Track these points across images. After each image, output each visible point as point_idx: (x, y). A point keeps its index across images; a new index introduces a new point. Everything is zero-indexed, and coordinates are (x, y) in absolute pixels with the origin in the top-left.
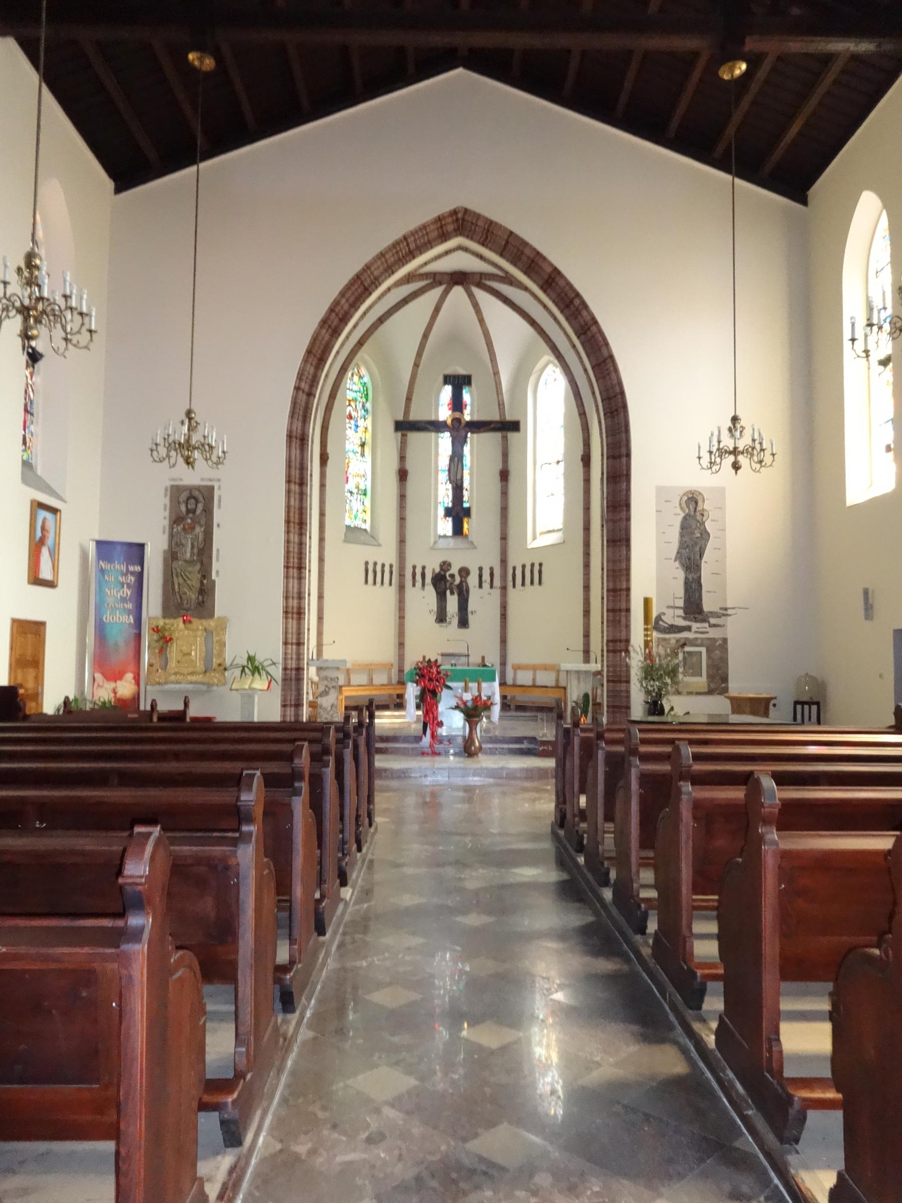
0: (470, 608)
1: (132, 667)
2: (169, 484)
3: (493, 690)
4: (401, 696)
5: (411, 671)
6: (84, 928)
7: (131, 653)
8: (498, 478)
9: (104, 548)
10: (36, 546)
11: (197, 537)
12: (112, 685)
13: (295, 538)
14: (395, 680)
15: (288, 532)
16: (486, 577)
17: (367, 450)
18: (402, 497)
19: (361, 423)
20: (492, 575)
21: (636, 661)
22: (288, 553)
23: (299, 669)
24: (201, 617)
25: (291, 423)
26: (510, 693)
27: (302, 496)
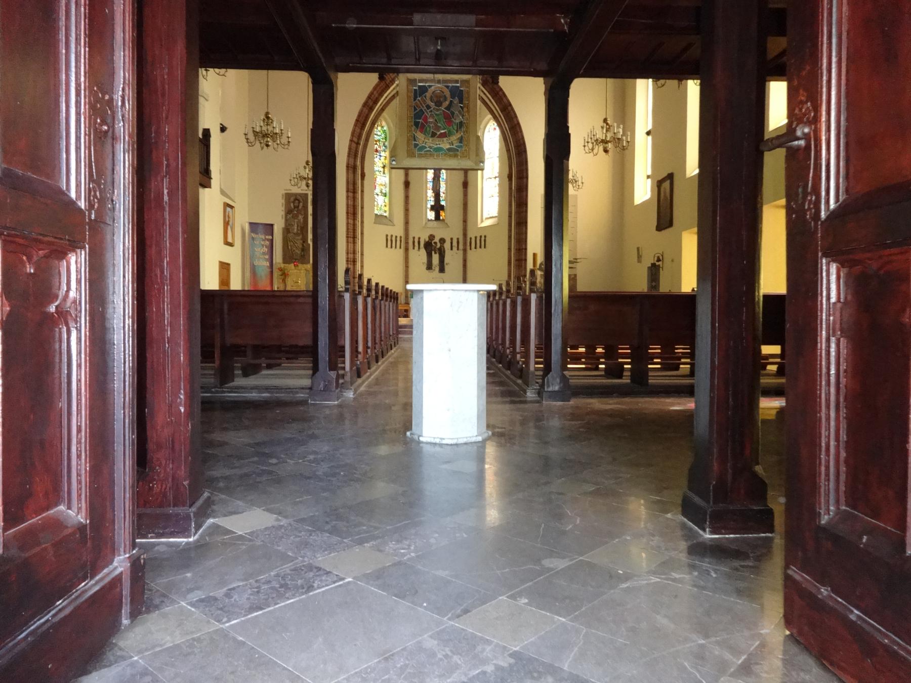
2: (284, 192)
6: (65, 617)
9: (254, 226)
10: (226, 224)
13: (351, 221)
15: (348, 218)
16: (455, 244)
18: (407, 197)
19: (383, 154)
22: (348, 229)
24: (302, 263)
25: (348, 160)
27: (354, 199)
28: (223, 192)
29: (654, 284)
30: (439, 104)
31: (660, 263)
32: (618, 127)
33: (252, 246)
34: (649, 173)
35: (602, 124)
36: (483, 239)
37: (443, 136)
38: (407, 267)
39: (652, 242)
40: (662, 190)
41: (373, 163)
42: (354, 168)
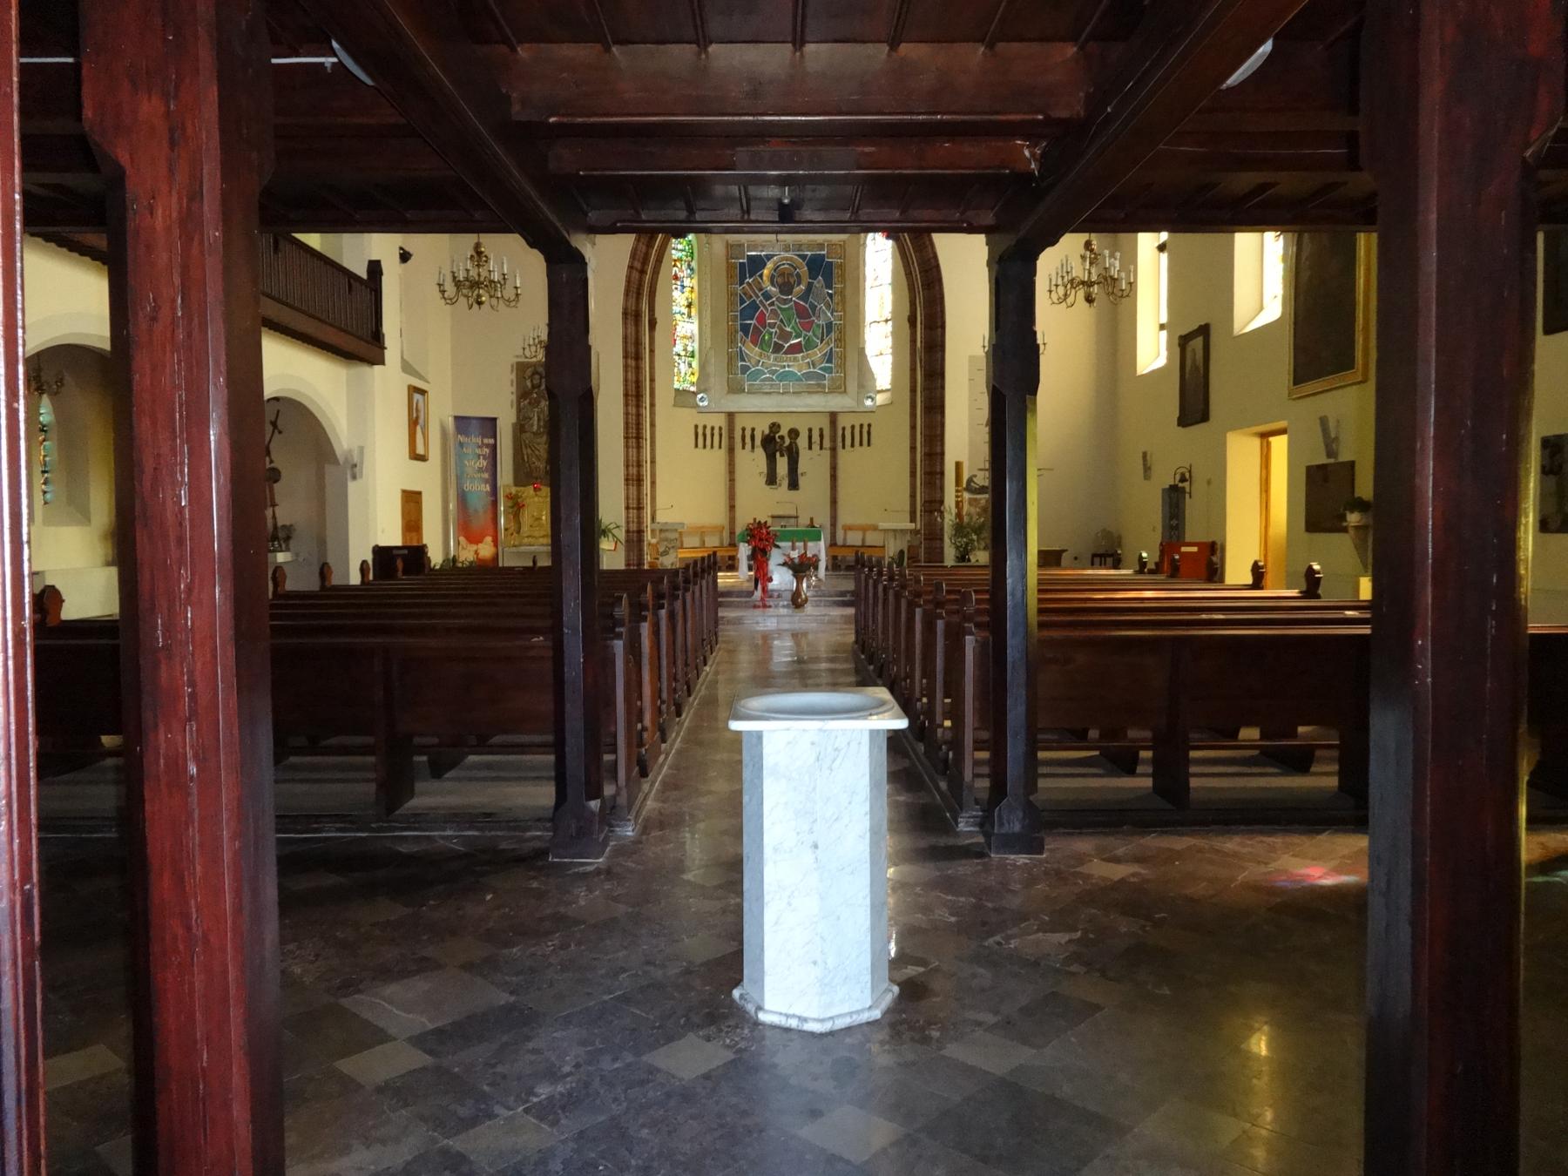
1: (491, 531)
3: (819, 549)
4: (733, 558)
5: (742, 534)
7: (490, 515)
9: (462, 422)
10: (413, 423)
12: (475, 547)
13: (632, 410)
14: (726, 542)
15: (626, 405)
16: (816, 438)
17: (694, 311)
19: (687, 282)
21: (949, 519)
22: (627, 424)
23: (640, 532)
26: (840, 553)
27: (638, 369)
28: (407, 368)
29: (1174, 522)
30: (786, 288)
31: (1186, 485)
32: (1112, 256)
33: (460, 457)
34: (1164, 320)
35: (1082, 251)
36: (865, 429)
37: (796, 349)
38: (732, 480)
39: (1177, 450)
40: (1189, 349)
41: (670, 301)
42: (637, 316)
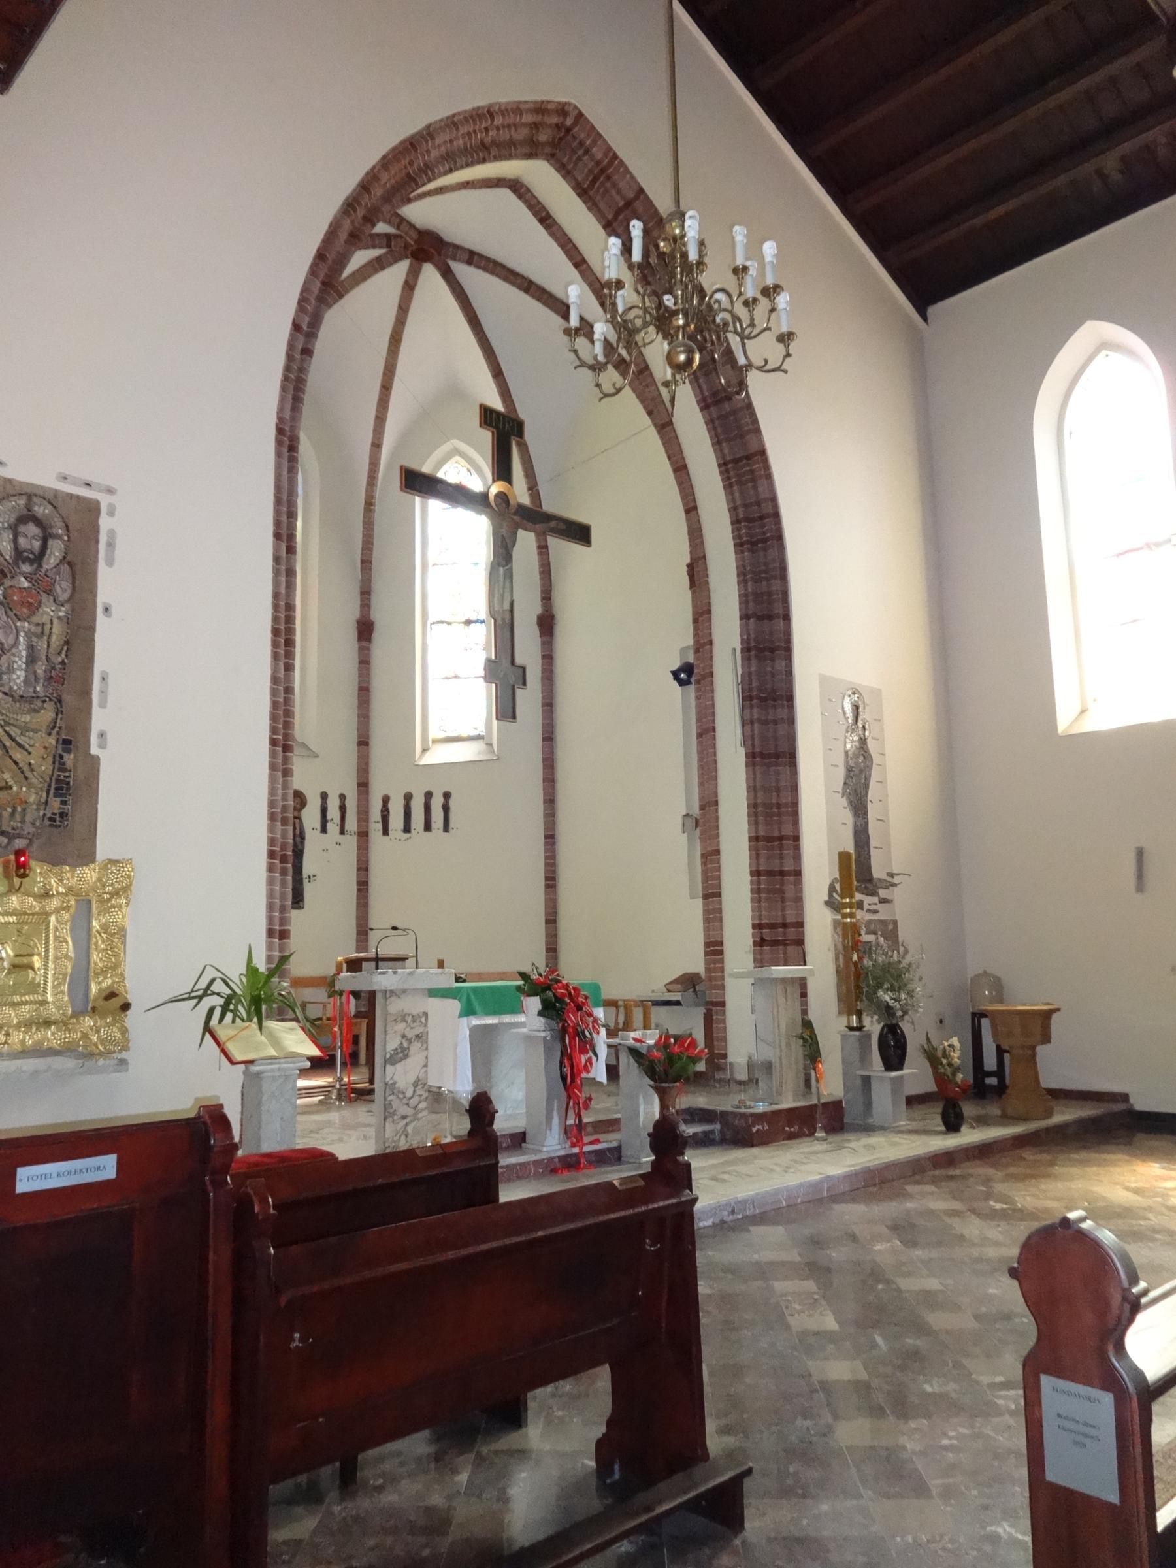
0: (307, 870)
8: (353, 634)
11: (42, 632)
16: (333, 813)
20: (343, 809)
24: (55, 861)
